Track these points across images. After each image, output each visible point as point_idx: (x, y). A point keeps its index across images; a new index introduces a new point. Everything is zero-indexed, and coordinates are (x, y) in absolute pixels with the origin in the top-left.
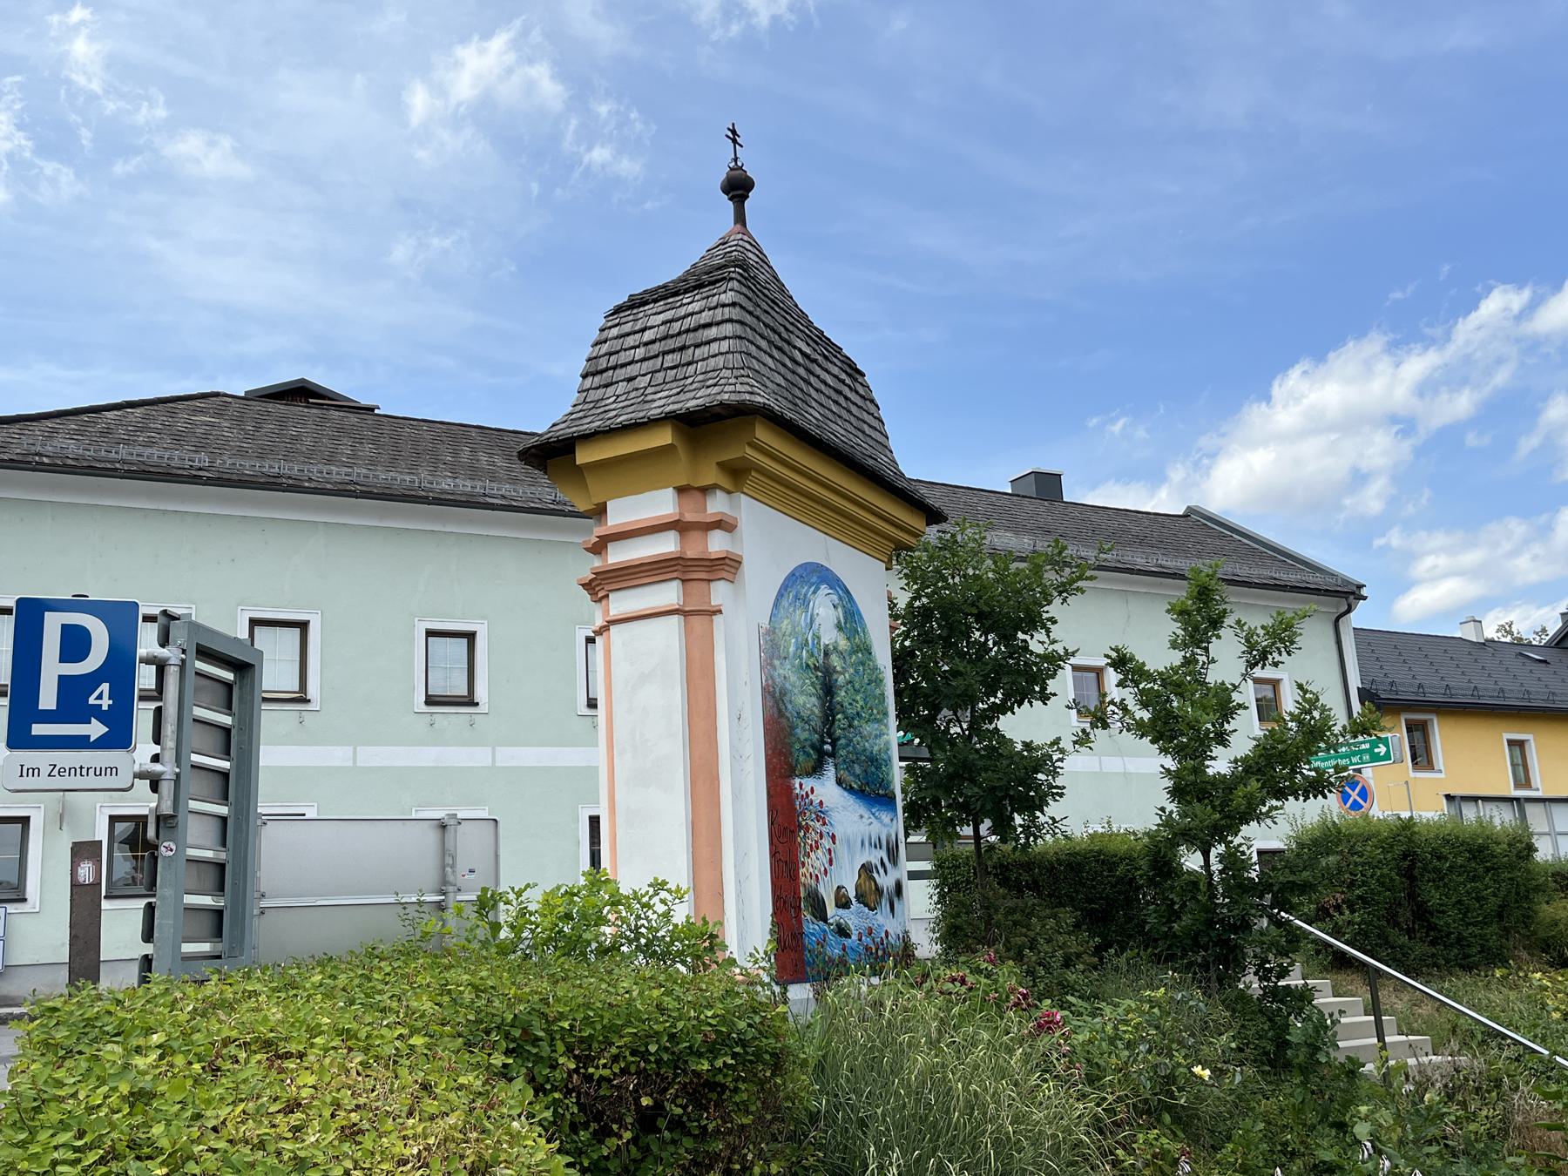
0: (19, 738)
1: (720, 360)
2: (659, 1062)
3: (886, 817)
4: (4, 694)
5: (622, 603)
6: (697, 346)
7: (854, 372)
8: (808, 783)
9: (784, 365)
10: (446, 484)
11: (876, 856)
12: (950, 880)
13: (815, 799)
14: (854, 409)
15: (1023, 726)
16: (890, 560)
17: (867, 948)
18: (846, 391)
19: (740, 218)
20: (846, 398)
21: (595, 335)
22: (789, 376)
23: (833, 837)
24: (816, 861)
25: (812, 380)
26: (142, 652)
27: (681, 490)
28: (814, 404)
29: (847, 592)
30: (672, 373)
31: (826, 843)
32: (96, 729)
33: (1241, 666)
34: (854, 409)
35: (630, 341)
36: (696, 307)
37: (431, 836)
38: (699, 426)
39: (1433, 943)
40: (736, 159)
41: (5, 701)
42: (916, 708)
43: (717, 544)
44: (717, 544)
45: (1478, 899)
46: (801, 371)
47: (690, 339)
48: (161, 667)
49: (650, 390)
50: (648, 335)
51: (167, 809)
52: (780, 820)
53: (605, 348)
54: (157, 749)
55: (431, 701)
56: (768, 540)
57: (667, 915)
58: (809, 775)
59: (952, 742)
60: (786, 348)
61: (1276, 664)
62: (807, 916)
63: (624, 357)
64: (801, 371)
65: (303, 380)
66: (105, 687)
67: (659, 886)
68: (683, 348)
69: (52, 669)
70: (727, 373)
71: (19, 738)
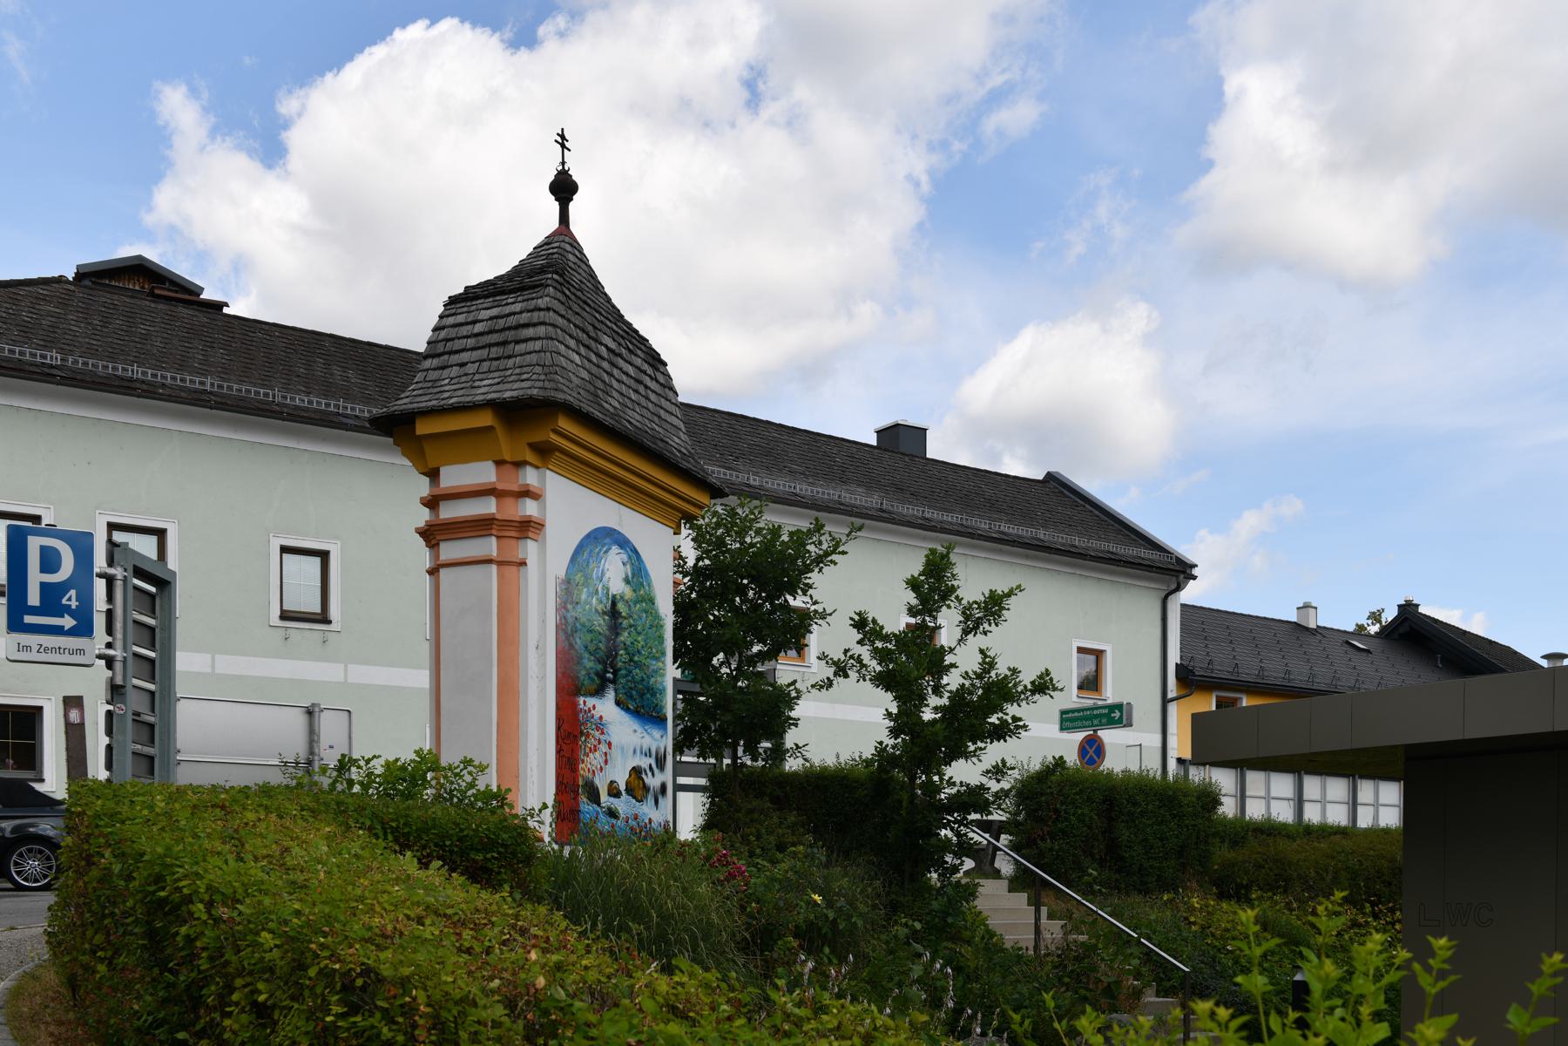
0: (15, 625)
1: (533, 358)
2: (451, 852)
3: (657, 733)
4: (1, 594)
5: (449, 551)
6: (517, 342)
7: (656, 361)
8: (591, 701)
9: (590, 361)
10: (299, 400)
11: (644, 762)
12: (720, 789)
13: (597, 714)
14: (653, 397)
15: (785, 671)
16: (679, 527)
17: (632, 829)
18: (647, 380)
19: (564, 217)
20: (646, 387)
21: (435, 320)
22: (594, 370)
23: (610, 744)
24: (595, 760)
25: (616, 372)
26: (96, 570)
27: (499, 463)
28: (615, 394)
29: (636, 552)
30: (495, 363)
31: (604, 748)
32: (68, 622)
33: (958, 632)
34: (653, 397)
35: (465, 330)
36: (518, 307)
37: (300, 719)
38: (516, 413)
39: (1119, 871)
40: (563, 163)
41: (3, 600)
42: (692, 651)
43: (530, 508)
44: (530, 508)
45: (1161, 839)
46: (605, 365)
47: (510, 335)
48: (110, 581)
49: (477, 377)
50: (478, 328)
51: (119, 681)
52: (565, 726)
53: (443, 334)
54: (110, 639)
55: (285, 616)
56: (568, 507)
57: (472, 785)
58: (592, 695)
59: (719, 679)
60: (593, 344)
61: (985, 633)
62: (583, 799)
63: (458, 344)
64: (605, 365)
65: (140, 257)
66: (73, 593)
67: (467, 762)
68: (504, 343)
69: (35, 578)
70: (538, 369)
71: (15, 625)
